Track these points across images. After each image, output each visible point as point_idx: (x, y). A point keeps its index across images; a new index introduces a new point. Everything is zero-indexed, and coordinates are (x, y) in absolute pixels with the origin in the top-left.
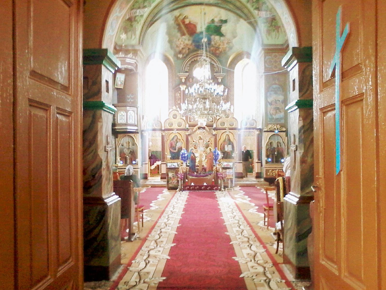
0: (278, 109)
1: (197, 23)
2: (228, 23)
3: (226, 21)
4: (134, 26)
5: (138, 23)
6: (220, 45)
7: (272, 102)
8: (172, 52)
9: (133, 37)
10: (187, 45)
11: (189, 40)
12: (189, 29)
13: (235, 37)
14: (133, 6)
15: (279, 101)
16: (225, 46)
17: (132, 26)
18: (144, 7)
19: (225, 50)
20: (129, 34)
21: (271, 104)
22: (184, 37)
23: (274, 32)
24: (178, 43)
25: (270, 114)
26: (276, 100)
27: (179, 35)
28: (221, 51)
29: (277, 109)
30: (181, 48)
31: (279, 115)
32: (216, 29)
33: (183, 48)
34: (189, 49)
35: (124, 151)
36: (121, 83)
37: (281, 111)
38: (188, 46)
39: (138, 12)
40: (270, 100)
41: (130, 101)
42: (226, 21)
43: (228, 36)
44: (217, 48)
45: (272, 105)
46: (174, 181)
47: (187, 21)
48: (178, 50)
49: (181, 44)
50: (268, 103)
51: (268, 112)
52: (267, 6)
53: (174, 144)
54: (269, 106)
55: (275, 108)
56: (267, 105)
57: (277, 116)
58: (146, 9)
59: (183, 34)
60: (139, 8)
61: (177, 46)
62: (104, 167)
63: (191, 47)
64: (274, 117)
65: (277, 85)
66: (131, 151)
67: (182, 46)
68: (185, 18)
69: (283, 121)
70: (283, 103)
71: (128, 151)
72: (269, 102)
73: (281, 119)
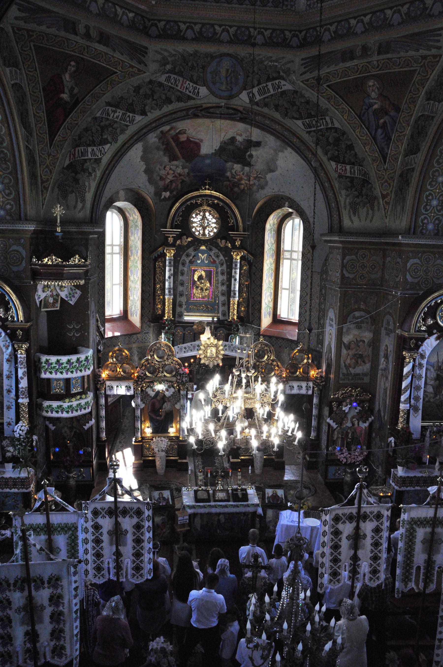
0: (361, 356)
1: (202, 141)
2: (261, 147)
3: (258, 144)
4: (81, 182)
5: (90, 174)
6: (241, 179)
7: (350, 343)
8: (152, 189)
9: (80, 205)
10: (180, 175)
11: (183, 168)
12: (189, 149)
13: (272, 171)
14: (80, 138)
15: (364, 341)
16: (251, 183)
17: (77, 181)
18: (104, 142)
19: (250, 189)
20: (72, 197)
21: (348, 347)
22: (175, 163)
23: (365, 209)
24: (163, 172)
25: (345, 366)
26: (359, 339)
27: (166, 159)
28: (244, 189)
29: (359, 358)
30: (168, 181)
31: (361, 367)
32: (238, 152)
33: (171, 182)
34: (183, 182)
35: (63, 431)
36: (54, 299)
37: (366, 361)
38: (182, 177)
39: (90, 152)
40: (346, 339)
41: (74, 328)
42: (258, 144)
43: (259, 166)
44: (237, 185)
45: (349, 349)
46: (164, 530)
47: (183, 138)
48: (161, 183)
49: (168, 174)
50: (343, 346)
51: (342, 362)
52: (356, 154)
53: (157, 405)
54: (344, 352)
55: (355, 355)
56: (341, 347)
57: (359, 370)
58: (107, 147)
59: (173, 158)
60: (93, 143)
61: (162, 179)
62: (22, 319)
63: (187, 179)
64: (352, 371)
65: (362, 312)
66: (75, 432)
67: (170, 177)
68: (180, 133)
69: (367, 380)
70: (370, 346)
71: (71, 432)
72: (344, 343)
73: (365, 374)
